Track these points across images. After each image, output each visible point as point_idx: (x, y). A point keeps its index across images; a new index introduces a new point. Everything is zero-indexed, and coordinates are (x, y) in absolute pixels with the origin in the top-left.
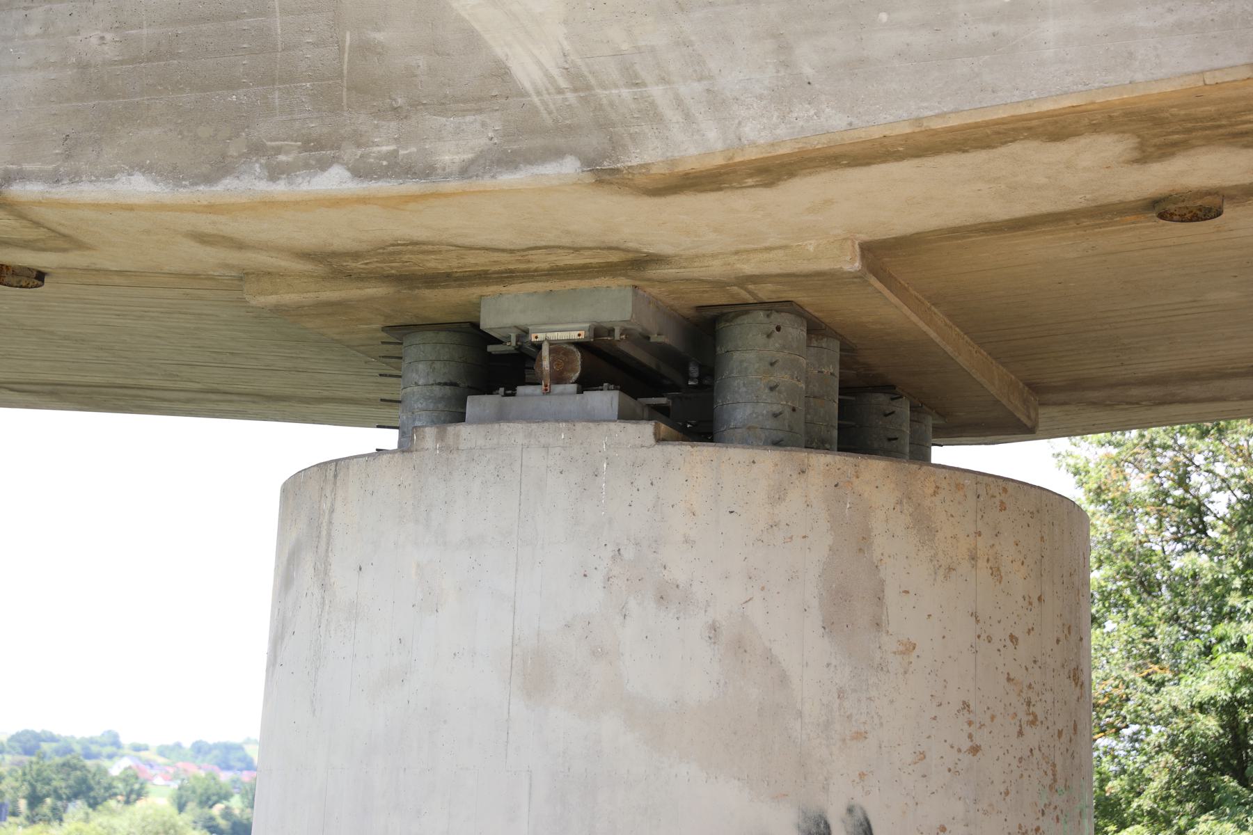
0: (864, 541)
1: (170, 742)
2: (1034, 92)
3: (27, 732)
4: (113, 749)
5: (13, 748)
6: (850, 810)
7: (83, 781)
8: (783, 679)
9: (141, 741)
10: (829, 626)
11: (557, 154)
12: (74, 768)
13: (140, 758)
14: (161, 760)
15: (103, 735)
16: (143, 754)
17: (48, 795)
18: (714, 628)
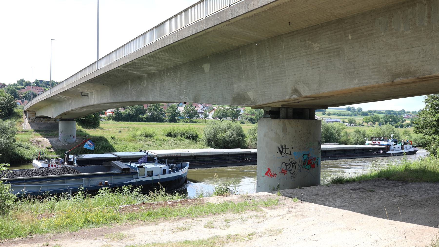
0: (285, 126)
1: (414, 111)
2: (316, 49)
3: (388, 110)
4: (404, 113)
5: (386, 113)
6: (284, 144)
7: (394, 119)
8: (279, 136)
9: (409, 111)
10: (282, 132)
11: (253, 104)
12: (392, 117)
13: (408, 114)
14: (412, 114)
15: (402, 110)
16: (409, 113)
17: (388, 121)
18: (275, 132)
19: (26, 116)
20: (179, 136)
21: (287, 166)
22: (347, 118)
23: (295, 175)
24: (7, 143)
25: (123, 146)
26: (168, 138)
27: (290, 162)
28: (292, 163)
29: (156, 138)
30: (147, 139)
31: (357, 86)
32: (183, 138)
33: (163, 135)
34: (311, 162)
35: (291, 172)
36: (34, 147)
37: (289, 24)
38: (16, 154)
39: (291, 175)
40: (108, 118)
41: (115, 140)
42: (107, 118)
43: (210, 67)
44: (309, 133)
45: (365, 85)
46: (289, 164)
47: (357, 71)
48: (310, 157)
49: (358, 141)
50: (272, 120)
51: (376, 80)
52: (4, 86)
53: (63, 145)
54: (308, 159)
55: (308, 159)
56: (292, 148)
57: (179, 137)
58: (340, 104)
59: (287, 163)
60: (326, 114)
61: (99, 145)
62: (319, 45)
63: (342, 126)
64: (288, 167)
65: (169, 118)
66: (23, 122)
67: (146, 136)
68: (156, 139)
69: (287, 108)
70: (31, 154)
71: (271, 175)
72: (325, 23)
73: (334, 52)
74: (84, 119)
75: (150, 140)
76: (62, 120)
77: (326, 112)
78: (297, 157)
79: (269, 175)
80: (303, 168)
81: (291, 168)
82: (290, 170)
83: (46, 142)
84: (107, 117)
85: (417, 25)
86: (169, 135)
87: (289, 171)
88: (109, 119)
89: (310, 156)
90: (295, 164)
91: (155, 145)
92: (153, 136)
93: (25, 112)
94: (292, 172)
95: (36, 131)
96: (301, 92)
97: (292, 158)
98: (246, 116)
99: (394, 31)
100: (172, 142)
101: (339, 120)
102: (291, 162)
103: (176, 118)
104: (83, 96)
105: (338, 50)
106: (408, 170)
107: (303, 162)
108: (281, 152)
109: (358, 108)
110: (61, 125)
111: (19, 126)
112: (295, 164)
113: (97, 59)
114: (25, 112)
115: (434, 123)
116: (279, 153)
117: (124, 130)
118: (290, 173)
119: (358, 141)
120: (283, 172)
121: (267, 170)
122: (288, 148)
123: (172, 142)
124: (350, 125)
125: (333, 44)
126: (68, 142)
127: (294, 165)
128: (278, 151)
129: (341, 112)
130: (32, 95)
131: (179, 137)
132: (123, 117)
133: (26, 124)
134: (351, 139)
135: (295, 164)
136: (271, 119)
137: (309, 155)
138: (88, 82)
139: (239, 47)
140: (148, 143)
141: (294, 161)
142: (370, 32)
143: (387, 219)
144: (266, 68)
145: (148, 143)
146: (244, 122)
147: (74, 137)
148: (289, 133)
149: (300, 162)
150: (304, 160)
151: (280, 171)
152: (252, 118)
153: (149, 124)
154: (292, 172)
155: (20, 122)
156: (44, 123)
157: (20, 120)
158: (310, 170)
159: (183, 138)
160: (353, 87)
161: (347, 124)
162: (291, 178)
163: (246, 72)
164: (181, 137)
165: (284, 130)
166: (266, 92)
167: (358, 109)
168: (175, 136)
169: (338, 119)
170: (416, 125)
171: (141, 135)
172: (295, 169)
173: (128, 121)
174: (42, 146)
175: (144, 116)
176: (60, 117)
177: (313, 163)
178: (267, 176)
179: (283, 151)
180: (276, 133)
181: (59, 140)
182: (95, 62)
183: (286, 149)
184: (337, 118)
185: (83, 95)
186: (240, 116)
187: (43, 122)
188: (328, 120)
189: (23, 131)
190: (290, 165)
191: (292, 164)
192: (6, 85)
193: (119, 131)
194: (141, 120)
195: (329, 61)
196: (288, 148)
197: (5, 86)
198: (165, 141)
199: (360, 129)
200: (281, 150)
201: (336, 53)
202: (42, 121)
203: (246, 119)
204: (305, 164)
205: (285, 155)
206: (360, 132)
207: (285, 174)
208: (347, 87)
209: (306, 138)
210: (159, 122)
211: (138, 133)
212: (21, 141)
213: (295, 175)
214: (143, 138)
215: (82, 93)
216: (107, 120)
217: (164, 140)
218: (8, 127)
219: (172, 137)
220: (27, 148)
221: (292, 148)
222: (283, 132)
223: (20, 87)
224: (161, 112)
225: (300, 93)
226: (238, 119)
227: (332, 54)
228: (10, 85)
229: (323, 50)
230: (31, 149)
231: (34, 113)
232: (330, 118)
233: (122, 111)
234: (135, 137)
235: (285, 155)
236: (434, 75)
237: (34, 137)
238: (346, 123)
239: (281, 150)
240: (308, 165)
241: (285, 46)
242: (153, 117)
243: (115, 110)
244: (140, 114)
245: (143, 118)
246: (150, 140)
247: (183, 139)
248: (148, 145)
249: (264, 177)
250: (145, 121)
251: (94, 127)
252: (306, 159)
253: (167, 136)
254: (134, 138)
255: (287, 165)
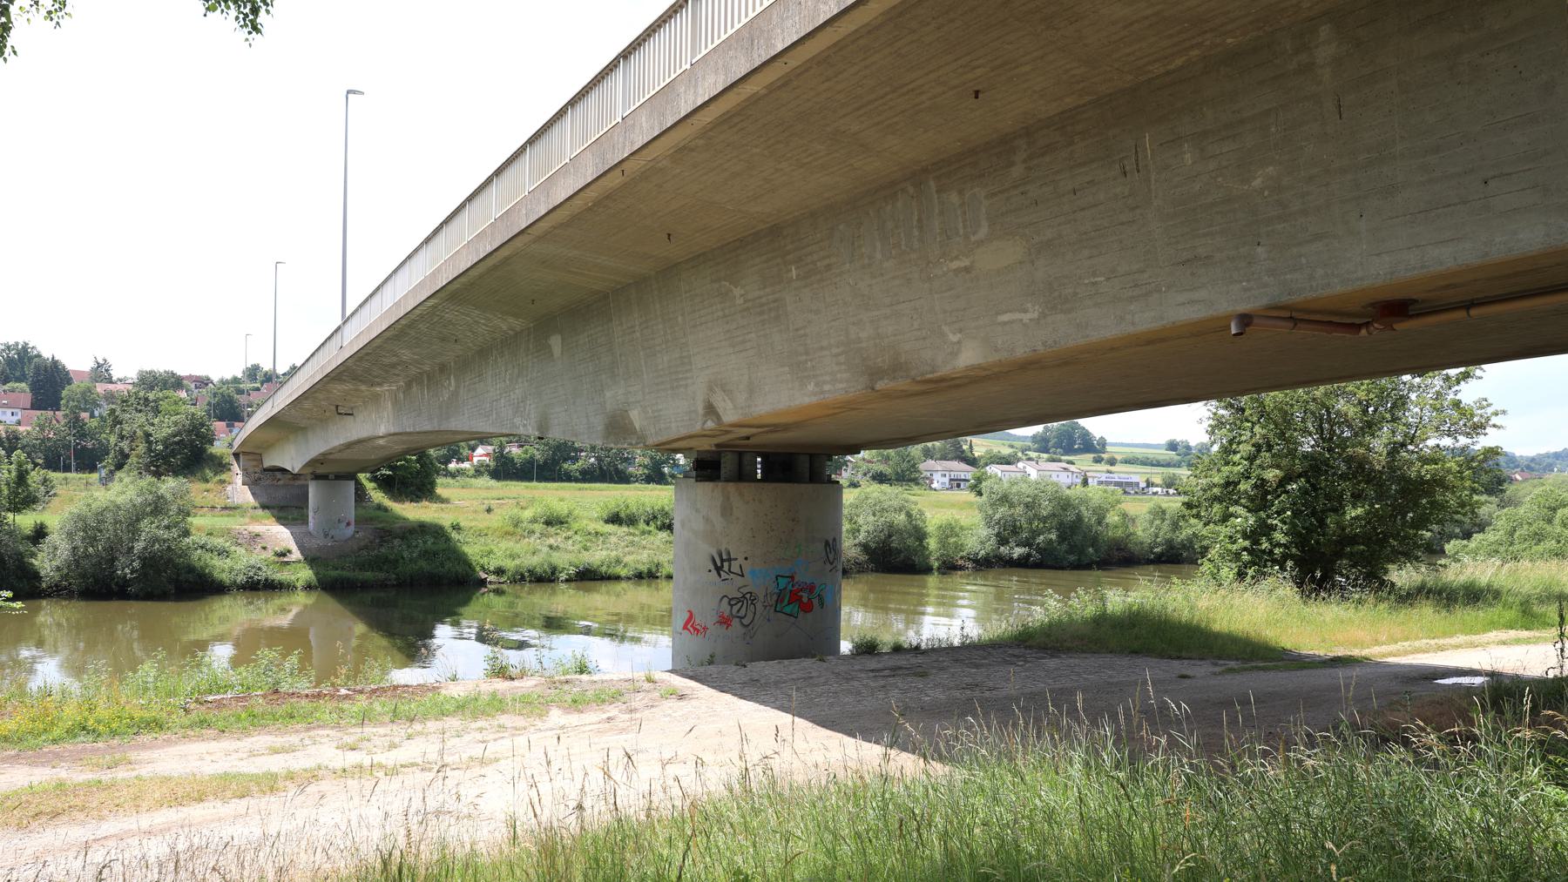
0: (728, 499)
6: (726, 549)
19: (239, 467)
20: (642, 521)
21: (732, 606)
22: (1159, 473)
23: (755, 630)
24: (164, 541)
25: (482, 548)
26: (610, 528)
27: (740, 595)
28: (746, 599)
29: (575, 526)
30: (552, 530)
31: (814, 399)
32: (652, 528)
33: (596, 520)
34: (801, 597)
35: (743, 621)
36: (241, 551)
37: (669, 239)
38: (191, 569)
39: (743, 630)
40: (476, 471)
41: (459, 534)
42: (472, 472)
43: (562, 343)
44: (793, 520)
45: (827, 396)
46: (739, 600)
47: (811, 360)
48: (797, 583)
49: (1159, 540)
50: (699, 483)
51: (844, 385)
52: (207, 384)
53: (318, 545)
54: (790, 587)
55: (790, 587)
56: (746, 559)
57: (642, 526)
58: (881, 441)
59: (733, 599)
60: (1103, 459)
61: (417, 546)
62: (743, 292)
63: (1112, 495)
64: (736, 608)
65: (646, 471)
66: (229, 483)
67: (548, 523)
68: (575, 529)
69: (740, 454)
70: (231, 570)
71: (695, 629)
72: (750, 235)
73: (770, 310)
74: (389, 475)
75: (557, 534)
76: (317, 477)
77: (1103, 455)
78: (758, 581)
79: (691, 629)
80: (775, 611)
81: (742, 612)
82: (741, 618)
83: (281, 535)
84: (473, 469)
85: (903, 247)
86: (615, 519)
87: (737, 620)
88: (478, 472)
89: (796, 580)
90: (753, 600)
91: (571, 548)
92: (567, 522)
93: (236, 455)
94: (746, 621)
95: (264, 507)
96: (721, 414)
97: (745, 586)
98: (864, 467)
99: (866, 261)
100: (620, 538)
101: (1135, 479)
102: (744, 596)
103: (666, 470)
104: (340, 414)
105: (776, 304)
106: (1102, 621)
107: (775, 597)
108: (718, 569)
109: (1198, 444)
110: (313, 491)
111: (218, 495)
112: (753, 600)
113: (343, 318)
114: (236, 455)
115: (1216, 491)
116: (714, 572)
117: (503, 504)
118: (742, 623)
119: (1159, 540)
120: (725, 621)
121: (687, 615)
122: (736, 559)
123: (620, 538)
124: (1167, 492)
125: (767, 290)
126: (332, 537)
127: (752, 603)
128: (712, 567)
129: (1149, 456)
130: (353, 405)
131: (642, 526)
132: (517, 469)
133: (239, 490)
134: (1140, 533)
135: (754, 602)
136: (697, 481)
137: (792, 578)
138: (333, 379)
139: (608, 293)
140: (551, 541)
141: (751, 593)
142: (827, 262)
143: (855, 737)
144: (658, 348)
145: (551, 541)
146: (858, 482)
147: (348, 524)
148: (738, 519)
149: (769, 596)
150: (781, 590)
151: (715, 619)
152: (881, 472)
153: (586, 489)
154: (746, 621)
155: (222, 482)
156: (284, 485)
157: (223, 477)
158: (796, 617)
159: (652, 528)
160: (807, 400)
161: (1159, 489)
162: (744, 638)
163: (623, 358)
164: (648, 524)
165: (726, 511)
166: (660, 410)
167: (1199, 447)
168: (631, 521)
169: (1131, 476)
170: (1185, 499)
171: (534, 520)
172: (755, 613)
173: (530, 479)
174: (264, 548)
175: (575, 467)
176: (309, 470)
177: (805, 600)
178: (686, 631)
179: (722, 566)
180: (707, 520)
181: (310, 533)
182: (338, 329)
183: (729, 560)
184: (1131, 473)
185: (339, 411)
186: (847, 466)
187: (281, 483)
188: (1103, 479)
189: (225, 508)
190: (741, 604)
191: (745, 601)
192: (212, 382)
193: (485, 507)
194: (568, 478)
195: (762, 333)
196: (736, 559)
197: (210, 385)
198: (602, 535)
199: (1164, 506)
200: (719, 565)
201: (773, 314)
202: (279, 480)
203: (865, 474)
204: (782, 601)
205: (727, 577)
206: (1164, 512)
207: (727, 628)
208: (797, 403)
209: (784, 532)
210: (616, 483)
211: (528, 514)
212: (211, 534)
213: (755, 630)
214: (538, 527)
215: (339, 408)
216: (474, 476)
217: (597, 533)
218: (169, 497)
219: (620, 524)
220: (223, 553)
221: (746, 559)
222: (722, 515)
223: (248, 385)
224: (623, 454)
225: (718, 417)
226: (841, 475)
227: (766, 317)
228: (223, 382)
229: (750, 304)
230: (231, 556)
231: (258, 457)
232: (1111, 473)
233: (514, 451)
234: (516, 526)
235: (727, 577)
236: (939, 374)
237: (246, 524)
238: (1157, 486)
239: (719, 565)
240: (789, 603)
241: (686, 292)
242: (601, 468)
243: (494, 450)
244: (565, 460)
245: (571, 471)
246: (557, 534)
247: (651, 531)
248: (551, 547)
249: (681, 634)
250: (577, 480)
251: (417, 497)
252: (786, 588)
253: (607, 522)
254: (515, 528)
255: (733, 602)
